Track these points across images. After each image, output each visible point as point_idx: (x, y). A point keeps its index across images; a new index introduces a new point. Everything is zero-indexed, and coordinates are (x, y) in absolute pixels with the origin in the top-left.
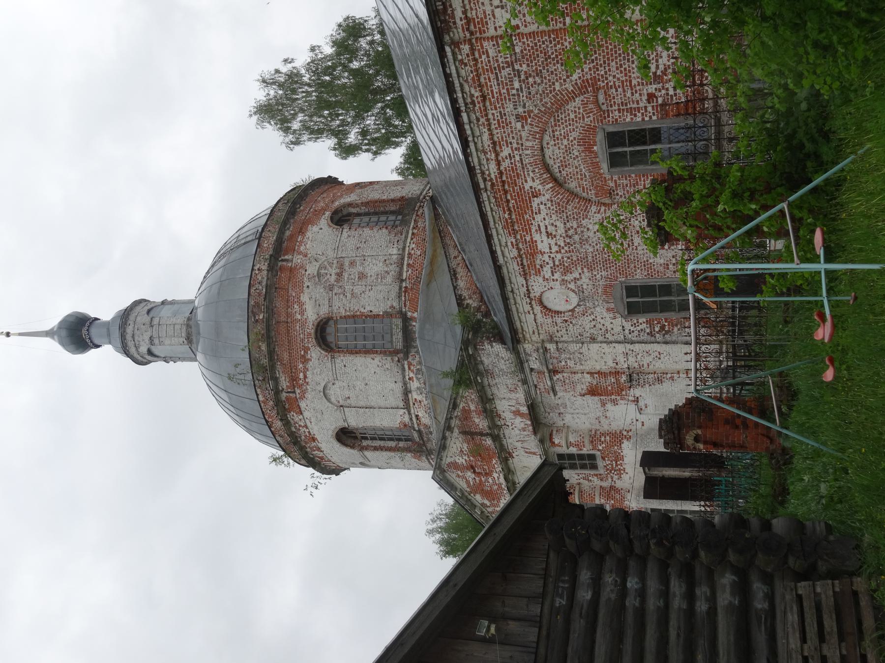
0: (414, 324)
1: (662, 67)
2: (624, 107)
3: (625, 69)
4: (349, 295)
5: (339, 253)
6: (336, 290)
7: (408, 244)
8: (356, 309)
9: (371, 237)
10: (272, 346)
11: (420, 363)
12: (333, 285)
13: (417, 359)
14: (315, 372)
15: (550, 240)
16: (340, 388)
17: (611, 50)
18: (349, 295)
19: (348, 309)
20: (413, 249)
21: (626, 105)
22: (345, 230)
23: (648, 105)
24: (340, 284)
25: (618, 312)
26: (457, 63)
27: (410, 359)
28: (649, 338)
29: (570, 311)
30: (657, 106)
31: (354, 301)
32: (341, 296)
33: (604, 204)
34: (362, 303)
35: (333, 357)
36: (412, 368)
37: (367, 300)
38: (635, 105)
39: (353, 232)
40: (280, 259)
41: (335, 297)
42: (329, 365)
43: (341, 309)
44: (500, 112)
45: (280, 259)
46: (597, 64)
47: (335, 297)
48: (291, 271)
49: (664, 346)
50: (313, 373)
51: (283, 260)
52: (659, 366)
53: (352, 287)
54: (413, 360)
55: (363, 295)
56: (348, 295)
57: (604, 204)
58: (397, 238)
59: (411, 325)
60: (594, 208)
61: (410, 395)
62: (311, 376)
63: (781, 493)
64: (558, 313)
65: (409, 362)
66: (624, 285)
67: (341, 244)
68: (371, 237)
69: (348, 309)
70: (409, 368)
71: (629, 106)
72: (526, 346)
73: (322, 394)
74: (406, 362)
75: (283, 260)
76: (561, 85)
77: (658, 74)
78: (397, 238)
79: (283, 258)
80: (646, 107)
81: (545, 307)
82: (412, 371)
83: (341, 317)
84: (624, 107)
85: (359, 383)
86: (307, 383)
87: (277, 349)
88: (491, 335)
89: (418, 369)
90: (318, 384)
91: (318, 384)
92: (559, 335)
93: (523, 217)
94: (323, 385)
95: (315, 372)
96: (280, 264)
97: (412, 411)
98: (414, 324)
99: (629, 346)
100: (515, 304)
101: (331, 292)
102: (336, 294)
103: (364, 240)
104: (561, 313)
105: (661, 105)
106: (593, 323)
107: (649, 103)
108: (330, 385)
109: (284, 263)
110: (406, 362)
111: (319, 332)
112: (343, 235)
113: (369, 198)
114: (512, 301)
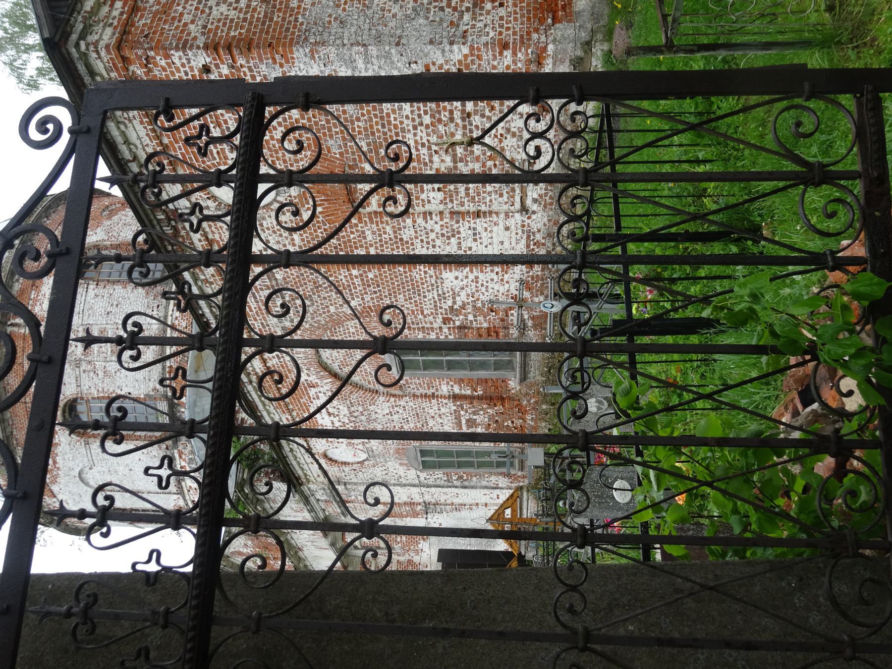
0: (183, 410)
1: (459, 303)
2: (415, 326)
3: (416, 302)
4: (101, 374)
5: (86, 318)
6: (84, 366)
7: (170, 313)
8: (111, 390)
9: (124, 298)
10: (9, 430)
11: (192, 452)
12: (80, 360)
13: (189, 448)
14: (66, 457)
15: (332, 418)
16: (99, 472)
17: (398, 285)
18: (101, 374)
19: (101, 389)
20: (176, 318)
21: (418, 324)
22: (91, 287)
23: (443, 326)
24: (89, 359)
25: (412, 466)
26: (200, 283)
27: (180, 448)
28: (446, 483)
29: (358, 463)
30: (454, 328)
31: (107, 380)
32: (92, 374)
33: (394, 396)
34: (118, 384)
35: (87, 443)
36: (184, 457)
37: (124, 380)
38: (428, 325)
39: (100, 291)
40: (9, 323)
41: (83, 375)
42: (83, 450)
43: (93, 389)
44: (262, 324)
45: (9, 323)
46: (381, 295)
47: (83, 375)
48: (24, 339)
49: (462, 490)
50: (64, 459)
51: (12, 325)
52: (457, 501)
53: (103, 364)
54: (185, 448)
55: (118, 374)
56: (99, 372)
57: (394, 396)
58: (156, 303)
59: (179, 411)
60: (382, 399)
61: (183, 484)
62: (61, 462)
63: (599, 215)
64: (345, 463)
65: (179, 451)
66: (418, 449)
67: (87, 306)
68: (124, 298)
69: (101, 389)
70: (180, 457)
71: (420, 325)
72: (311, 486)
73: (78, 479)
74: (176, 451)
75: (12, 325)
76: (337, 308)
77: (455, 307)
78: (156, 303)
79: (12, 321)
80: (441, 328)
81: (331, 459)
82: (184, 460)
83: (93, 398)
84: (415, 326)
85: (121, 468)
86: (58, 469)
87: (15, 433)
88: (270, 470)
89: (191, 459)
90: (72, 469)
91: (72, 469)
92: (348, 478)
93: (299, 401)
94: (77, 471)
95: (66, 457)
96: (9, 329)
97: (187, 498)
98: (183, 410)
99: (423, 489)
100: (296, 458)
101: (77, 369)
102: (84, 371)
103: (115, 303)
104: (349, 464)
105: (460, 328)
106: (385, 472)
107: (445, 324)
108: (87, 469)
109: (15, 329)
110: (176, 451)
111: (67, 411)
112: (89, 294)
113: (120, 239)
114: (291, 458)
